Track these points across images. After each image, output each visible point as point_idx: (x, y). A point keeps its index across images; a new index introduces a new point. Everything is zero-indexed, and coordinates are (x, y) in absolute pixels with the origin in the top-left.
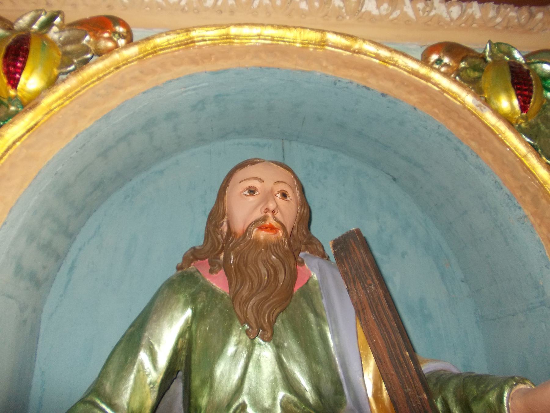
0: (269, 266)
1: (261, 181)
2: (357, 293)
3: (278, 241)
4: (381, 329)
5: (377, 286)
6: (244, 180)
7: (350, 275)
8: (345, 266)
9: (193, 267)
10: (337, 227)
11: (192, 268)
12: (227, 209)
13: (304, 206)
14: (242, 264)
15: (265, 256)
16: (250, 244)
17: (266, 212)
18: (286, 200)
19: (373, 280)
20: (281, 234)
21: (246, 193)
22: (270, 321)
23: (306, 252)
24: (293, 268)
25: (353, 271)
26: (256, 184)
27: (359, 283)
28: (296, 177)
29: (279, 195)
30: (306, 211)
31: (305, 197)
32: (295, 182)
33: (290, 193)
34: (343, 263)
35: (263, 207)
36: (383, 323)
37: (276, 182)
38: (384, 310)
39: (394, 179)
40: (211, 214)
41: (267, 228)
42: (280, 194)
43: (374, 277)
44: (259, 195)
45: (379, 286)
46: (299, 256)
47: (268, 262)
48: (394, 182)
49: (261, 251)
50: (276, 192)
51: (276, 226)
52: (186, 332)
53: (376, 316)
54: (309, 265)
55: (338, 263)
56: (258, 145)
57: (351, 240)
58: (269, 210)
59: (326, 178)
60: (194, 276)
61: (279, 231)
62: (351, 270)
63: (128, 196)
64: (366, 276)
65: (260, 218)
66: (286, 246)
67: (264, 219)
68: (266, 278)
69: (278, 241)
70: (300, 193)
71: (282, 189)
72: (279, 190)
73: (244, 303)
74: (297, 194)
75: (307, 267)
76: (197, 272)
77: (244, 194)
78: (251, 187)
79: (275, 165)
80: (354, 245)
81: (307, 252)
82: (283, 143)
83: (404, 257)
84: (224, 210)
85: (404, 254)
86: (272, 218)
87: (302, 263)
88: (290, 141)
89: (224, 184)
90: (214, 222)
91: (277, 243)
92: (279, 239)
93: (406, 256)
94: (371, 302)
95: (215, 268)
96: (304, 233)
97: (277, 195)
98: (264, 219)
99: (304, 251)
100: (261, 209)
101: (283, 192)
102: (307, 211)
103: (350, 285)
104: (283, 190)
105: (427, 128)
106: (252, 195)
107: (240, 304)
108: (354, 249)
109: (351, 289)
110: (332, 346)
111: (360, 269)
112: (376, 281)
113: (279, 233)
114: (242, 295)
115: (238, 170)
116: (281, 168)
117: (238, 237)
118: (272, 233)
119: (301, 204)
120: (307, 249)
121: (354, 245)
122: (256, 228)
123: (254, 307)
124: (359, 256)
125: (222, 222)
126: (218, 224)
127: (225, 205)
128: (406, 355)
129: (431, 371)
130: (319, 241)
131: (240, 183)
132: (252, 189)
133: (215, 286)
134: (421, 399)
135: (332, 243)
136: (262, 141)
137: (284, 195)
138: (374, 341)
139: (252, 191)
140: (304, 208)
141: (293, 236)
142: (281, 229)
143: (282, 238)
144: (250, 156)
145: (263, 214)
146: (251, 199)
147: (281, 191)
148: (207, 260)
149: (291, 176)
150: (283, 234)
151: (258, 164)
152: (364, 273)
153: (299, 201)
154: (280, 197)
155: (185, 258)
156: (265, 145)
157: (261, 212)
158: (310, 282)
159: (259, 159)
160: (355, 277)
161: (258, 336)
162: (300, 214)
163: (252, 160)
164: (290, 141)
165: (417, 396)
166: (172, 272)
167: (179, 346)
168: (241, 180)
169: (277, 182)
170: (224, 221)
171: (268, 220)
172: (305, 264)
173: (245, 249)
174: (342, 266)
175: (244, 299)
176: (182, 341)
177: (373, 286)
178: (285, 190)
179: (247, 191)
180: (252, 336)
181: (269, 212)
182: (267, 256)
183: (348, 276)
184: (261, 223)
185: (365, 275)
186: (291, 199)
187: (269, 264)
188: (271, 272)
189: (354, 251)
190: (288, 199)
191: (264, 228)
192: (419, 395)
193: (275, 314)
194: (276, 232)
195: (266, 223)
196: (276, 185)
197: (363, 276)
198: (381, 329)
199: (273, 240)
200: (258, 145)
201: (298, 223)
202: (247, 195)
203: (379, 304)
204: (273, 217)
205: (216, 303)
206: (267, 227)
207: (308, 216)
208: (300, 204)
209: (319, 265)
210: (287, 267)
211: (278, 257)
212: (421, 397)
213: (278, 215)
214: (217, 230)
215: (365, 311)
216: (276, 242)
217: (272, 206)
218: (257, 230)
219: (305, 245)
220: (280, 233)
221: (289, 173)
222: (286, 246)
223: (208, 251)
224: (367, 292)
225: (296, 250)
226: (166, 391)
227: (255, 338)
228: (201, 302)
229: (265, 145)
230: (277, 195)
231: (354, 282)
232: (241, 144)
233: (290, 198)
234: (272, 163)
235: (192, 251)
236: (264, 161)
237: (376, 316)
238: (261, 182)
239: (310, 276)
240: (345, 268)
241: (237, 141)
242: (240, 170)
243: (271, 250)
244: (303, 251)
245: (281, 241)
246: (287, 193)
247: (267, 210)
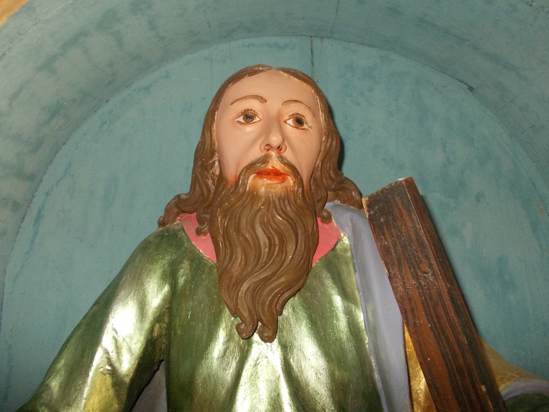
0: (272, 232)
1: (262, 100)
2: (404, 283)
3: (287, 192)
4: (441, 344)
5: (438, 276)
6: (241, 99)
7: (393, 255)
8: (386, 239)
9: (179, 222)
10: (384, 160)
11: (177, 224)
12: (216, 144)
13: (332, 136)
14: (231, 230)
15: (265, 216)
16: (244, 198)
17: (268, 150)
18: (302, 129)
19: (431, 266)
20: (292, 182)
21: (241, 119)
22: (273, 312)
23: (336, 201)
24: (310, 229)
25: (399, 248)
26: (255, 105)
27: (407, 268)
28: (319, 92)
29: (291, 122)
30: (334, 143)
31: (334, 123)
32: (318, 99)
33: (308, 117)
34: (384, 234)
35: (263, 142)
36: (444, 334)
37: (285, 102)
38: (447, 314)
39: (471, 89)
40: (197, 152)
41: (269, 175)
42: (292, 119)
43: (433, 262)
44: (260, 122)
45: (441, 277)
46: (325, 207)
47: (271, 225)
48: (471, 93)
49: (259, 210)
50: (286, 118)
51: (282, 171)
52: (164, 315)
53: (434, 323)
54: (337, 222)
55: (376, 234)
56: (277, 45)
57: (397, 199)
58: (272, 147)
59: (371, 90)
60: (177, 236)
61: (289, 177)
62: (395, 246)
63: (106, 123)
64: (419, 258)
65: (260, 159)
66: (299, 199)
67: (265, 160)
68: (267, 250)
69: (287, 192)
70: (325, 116)
71: (296, 112)
72: (291, 114)
73: (235, 286)
74: (320, 119)
75: (335, 224)
76: (182, 231)
77: (237, 121)
78: (248, 110)
79: (286, 75)
80: (401, 206)
81: (337, 202)
84: (212, 144)
85: (479, 197)
86: (276, 159)
87: (328, 219)
88: (322, 38)
89: (212, 107)
90: (200, 163)
91: (284, 196)
92: (289, 189)
93: (482, 200)
94: (425, 298)
95: (203, 227)
96: (330, 175)
97: (288, 122)
98: (265, 160)
99: (332, 200)
100: (260, 147)
101: (298, 116)
102: (337, 143)
103: (393, 270)
104: (298, 114)
105: (533, 4)
106: (249, 122)
107: (228, 287)
108: (401, 213)
109: (395, 275)
111: (411, 247)
112: (435, 266)
113: (289, 181)
114: (231, 275)
115: (231, 84)
116: (296, 79)
117: (229, 187)
118: (276, 182)
119: (327, 134)
120: (337, 197)
121: (401, 206)
122: (253, 174)
123: (249, 294)
124: (410, 224)
125: (211, 162)
126: (205, 164)
127: (213, 139)
128: (481, 389)
129: (517, 396)
130: (355, 185)
131: (232, 104)
133: (201, 254)
135: (367, 201)
136: (282, 41)
137: (299, 121)
138: (429, 359)
139: (249, 117)
140: (332, 138)
141: (315, 180)
142: (291, 175)
143: (294, 189)
144: (249, 63)
145: (265, 152)
146: (249, 128)
147: (293, 114)
148: (195, 214)
149: (312, 92)
150: (294, 183)
151: (261, 74)
152: (417, 252)
153: (324, 128)
154: (292, 124)
155: (168, 211)
156: (286, 46)
157: (261, 149)
158: (339, 247)
159: (263, 66)
160: (402, 258)
161: (256, 332)
162: (325, 146)
163: (252, 68)
164: (322, 38)
166: (153, 228)
167: (155, 334)
168: (234, 100)
169: (287, 102)
170: (215, 161)
171: (270, 163)
172: (333, 220)
173: (236, 205)
174: (381, 239)
175: (234, 280)
176: (160, 327)
177: (430, 274)
178: (299, 113)
179: (242, 117)
180: (244, 335)
181: (272, 150)
182: (269, 216)
183: (391, 254)
184: (262, 167)
185: (418, 256)
186: (311, 127)
187: (272, 228)
188: (274, 241)
189: (402, 216)
190: (305, 126)
191: (265, 175)
193: (280, 302)
194: (284, 180)
195: (268, 167)
196: (285, 106)
197: (415, 257)
198: (441, 344)
200: (277, 45)
201: (323, 162)
202: (243, 123)
203: (440, 304)
204: (278, 157)
205: (202, 278)
206: (269, 173)
207: (338, 150)
208: (325, 133)
209: (352, 222)
210: (300, 232)
211: (286, 218)
213: (288, 154)
214: (206, 173)
215: (416, 313)
216: (283, 194)
217: (275, 140)
218: (254, 177)
219: (334, 190)
220: (290, 181)
221: (308, 86)
222: (298, 200)
223: (196, 202)
224: (420, 283)
225: (319, 201)
226: (146, 385)
227: (253, 334)
228: (183, 276)
229: (286, 46)
230: (288, 122)
231: (400, 265)
232: (253, 45)
233: (309, 125)
234: (281, 72)
235: (176, 200)
236: (270, 68)
237: (434, 323)
238: (263, 103)
239: (339, 238)
240: (386, 243)
241: (247, 41)
242: (233, 84)
243: (276, 208)
244: (330, 201)
245: (292, 192)
247: (269, 147)
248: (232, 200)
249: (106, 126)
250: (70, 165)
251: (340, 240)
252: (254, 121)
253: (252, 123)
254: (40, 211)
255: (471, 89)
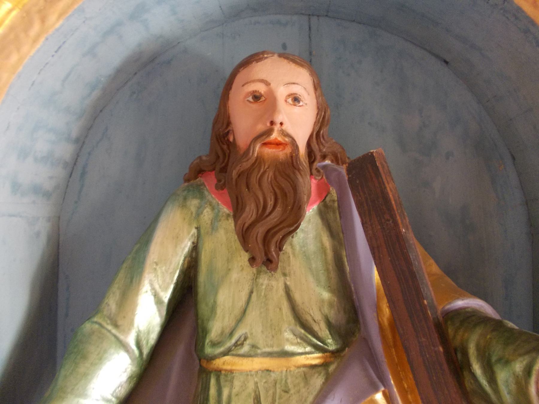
10: (369, 124)
21: (250, 99)
39: (446, 62)
63: (134, 93)
82: (309, 19)
83: (447, 158)
88: (318, 16)
101: (295, 95)
110: (348, 272)
115: (242, 69)
131: (243, 86)
132: (257, 94)
134: (435, 352)
135: (347, 167)
136: (283, 18)
165: (432, 348)
174: (357, 196)
177: (391, 222)
192: (434, 346)
199: (280, 157)
212: (436, 349)
242: (243, 69)
246: (300, 97)
248: (249, 246)
249: (135, 96)
250: (107, 129)
251: (329, 193)
252: (261, 100)
253: (260, 102)
254: (84, 168)
255: (446, 62)
